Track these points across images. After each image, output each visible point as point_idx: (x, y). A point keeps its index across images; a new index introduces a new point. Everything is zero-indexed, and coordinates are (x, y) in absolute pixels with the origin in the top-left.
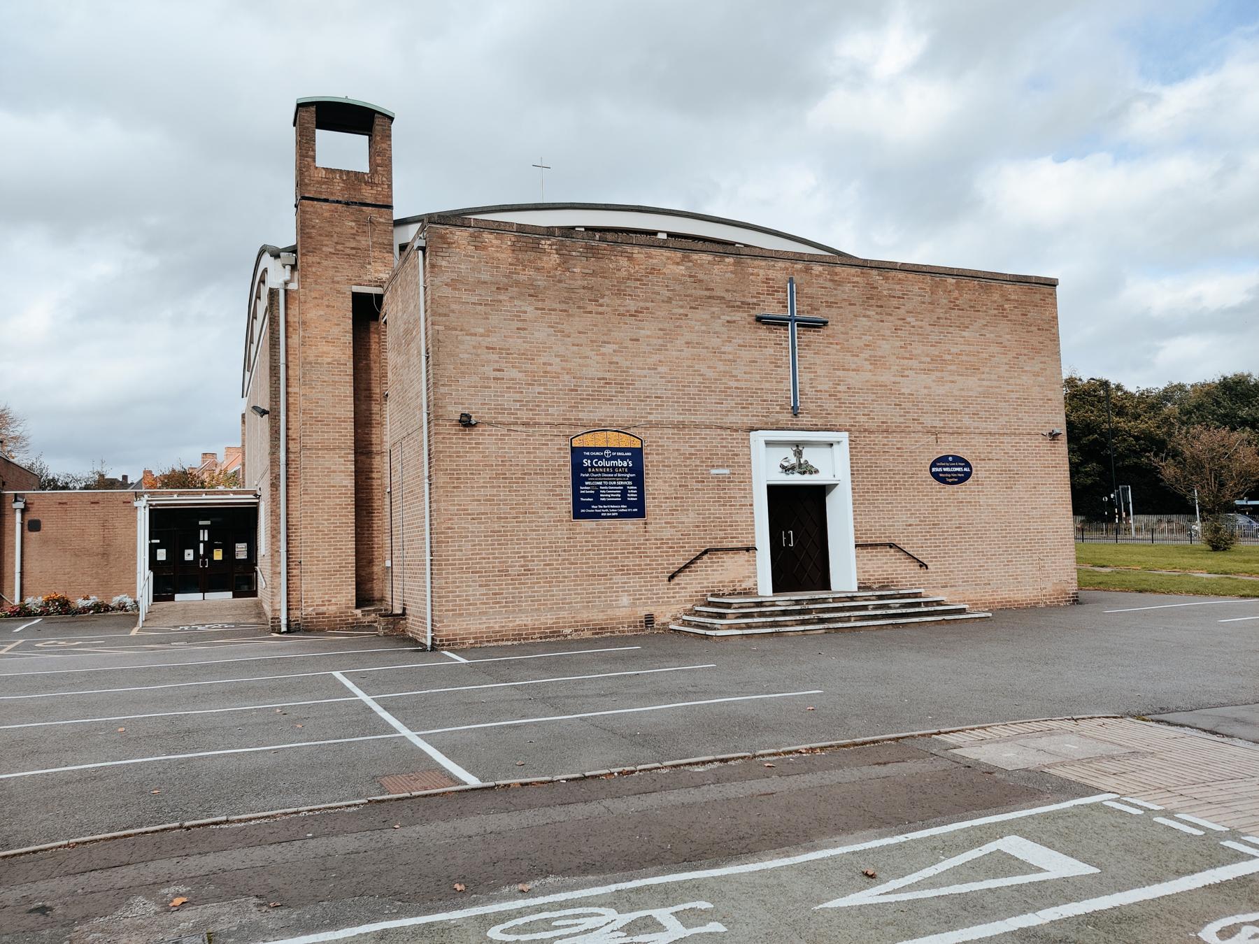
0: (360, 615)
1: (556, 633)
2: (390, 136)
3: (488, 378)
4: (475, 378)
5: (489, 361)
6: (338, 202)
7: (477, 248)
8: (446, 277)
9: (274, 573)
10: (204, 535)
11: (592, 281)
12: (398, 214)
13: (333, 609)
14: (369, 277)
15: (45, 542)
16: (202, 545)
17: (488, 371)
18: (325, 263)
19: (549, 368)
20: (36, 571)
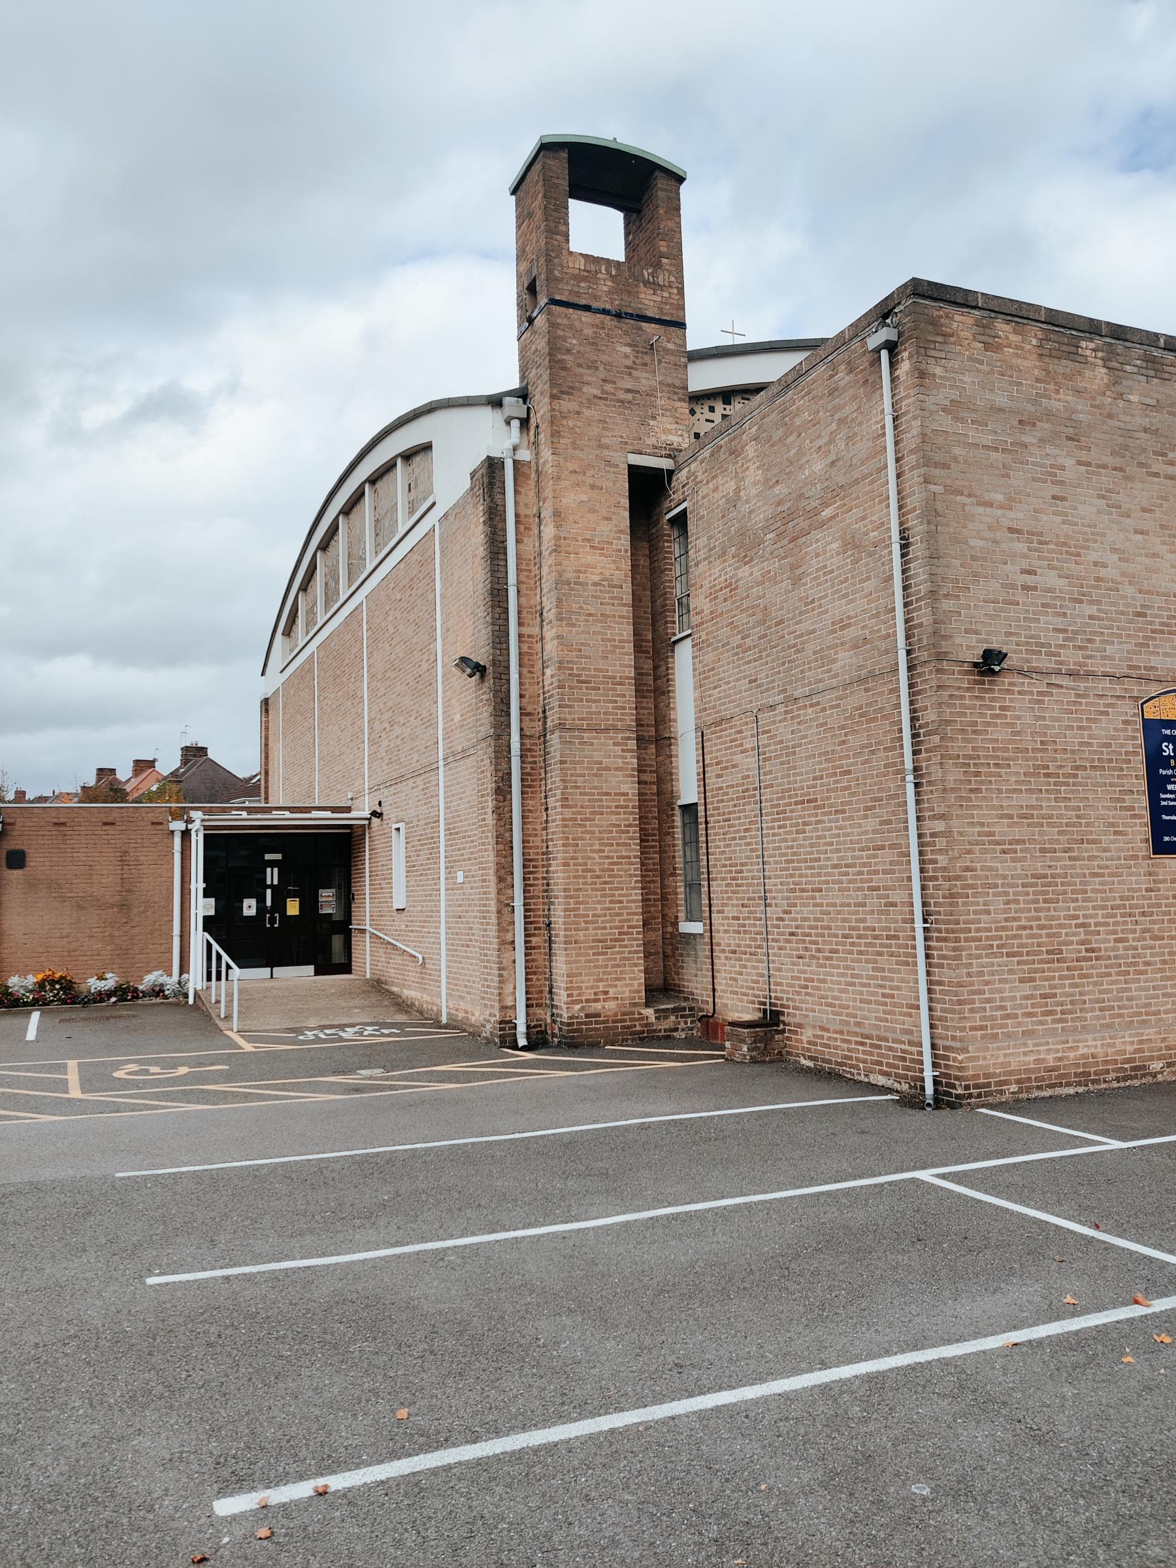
0: (652, 1019)
1: (1140, 1070)
2: (679, 209)
3: (1013, 586)
4: (995, 585)
5: (1013, 555)
6: (605, 312)
7: (987, 346)
8: (943, 396)
9: (503, 943)
10: (272, 876)
11: (1158, 419)
12: (694, 342)
13: (611, 1005)
14: (652, 441)
15: (32, 885)
16: (269, 892)
17: (1012, 570)
18: (587, 413)
19: (1103, 572)
20: (38, 931)
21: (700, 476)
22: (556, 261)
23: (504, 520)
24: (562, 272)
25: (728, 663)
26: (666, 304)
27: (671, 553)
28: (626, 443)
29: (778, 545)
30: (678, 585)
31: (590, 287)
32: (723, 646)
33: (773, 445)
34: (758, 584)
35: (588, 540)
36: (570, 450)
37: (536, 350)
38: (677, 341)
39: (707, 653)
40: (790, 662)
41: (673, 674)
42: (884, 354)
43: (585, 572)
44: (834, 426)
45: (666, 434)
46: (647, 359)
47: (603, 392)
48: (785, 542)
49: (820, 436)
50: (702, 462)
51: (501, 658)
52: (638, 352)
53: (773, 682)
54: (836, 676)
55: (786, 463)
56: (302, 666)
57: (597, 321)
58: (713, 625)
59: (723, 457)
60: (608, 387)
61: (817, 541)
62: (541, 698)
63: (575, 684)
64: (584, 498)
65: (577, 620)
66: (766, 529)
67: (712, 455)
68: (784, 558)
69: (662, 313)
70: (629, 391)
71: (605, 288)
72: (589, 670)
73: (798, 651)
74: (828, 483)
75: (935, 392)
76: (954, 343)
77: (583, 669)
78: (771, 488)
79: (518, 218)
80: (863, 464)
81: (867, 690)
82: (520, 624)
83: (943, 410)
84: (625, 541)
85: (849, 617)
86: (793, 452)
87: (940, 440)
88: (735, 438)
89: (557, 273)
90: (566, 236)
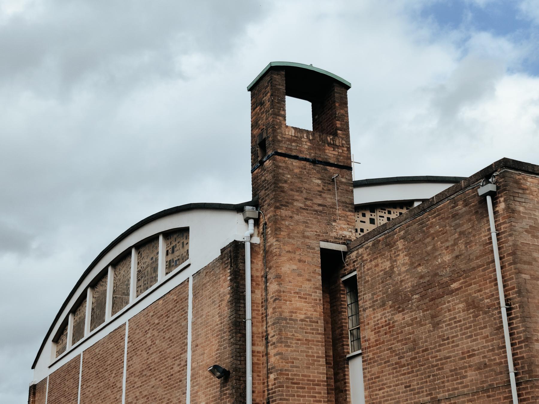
14: (334, 234)
18: (296, 217)
21: (365, 257)
22: (278, 131)
23: (244, 279)
24: (282, 137)
25: (389, 374)
26: (340, 156)
27: (345, 301)
28: (319, 235)
29: (422, 302)
30: (350, 322)
31: (297, 146)
32: (385, 363)
33: (415, 243)
34: (409, 325)
35: (297, 293)
36: (286, 239)
37: (265, 180)
38: (347, 177)
39: (374, 366)
40: (433, 376)
41: (348, 379)
42: (489, 199)
43: (296, 313)
44: (456, 236)
45: (347, 229)
46: (330, 187)
47: (306, 205)
48: (427, 300)
49: (447, 241)
50: (366, 248)
51: (240, 366)
52: (325, 183)
53: (422, 388)
54: (466, 386)
55: (425, 254)
56: (69, 364)
57: (302, 165)
58: (378, 349)
59: (381, 246)
60: (308, 203)
61: (449, 302)
62: (266, 393)
63: (290, 385)
64: (295, 267)
65: (291, 343)
66: (413, 292)
67: (373, 245)
68: (427, 310)
69: (339, 161)
70: (320, 205)
71: (306, 147)
72: (299, 375)
73: (439, 369)
74: (455, 268)
75: (520, 221)
76: (529, 194)
77: (295, 375)
78: (415, 268)
79: (252, 104)
80: (477, 258)
81: (489, 397)
82: (253, 344)
83: (526, 231)
84: (319, 294)
85: (474, 350)
86: (429, 248)
87: (526, 249)
88: (389, 236)
89: (279, 138)
90: (284, 117)
